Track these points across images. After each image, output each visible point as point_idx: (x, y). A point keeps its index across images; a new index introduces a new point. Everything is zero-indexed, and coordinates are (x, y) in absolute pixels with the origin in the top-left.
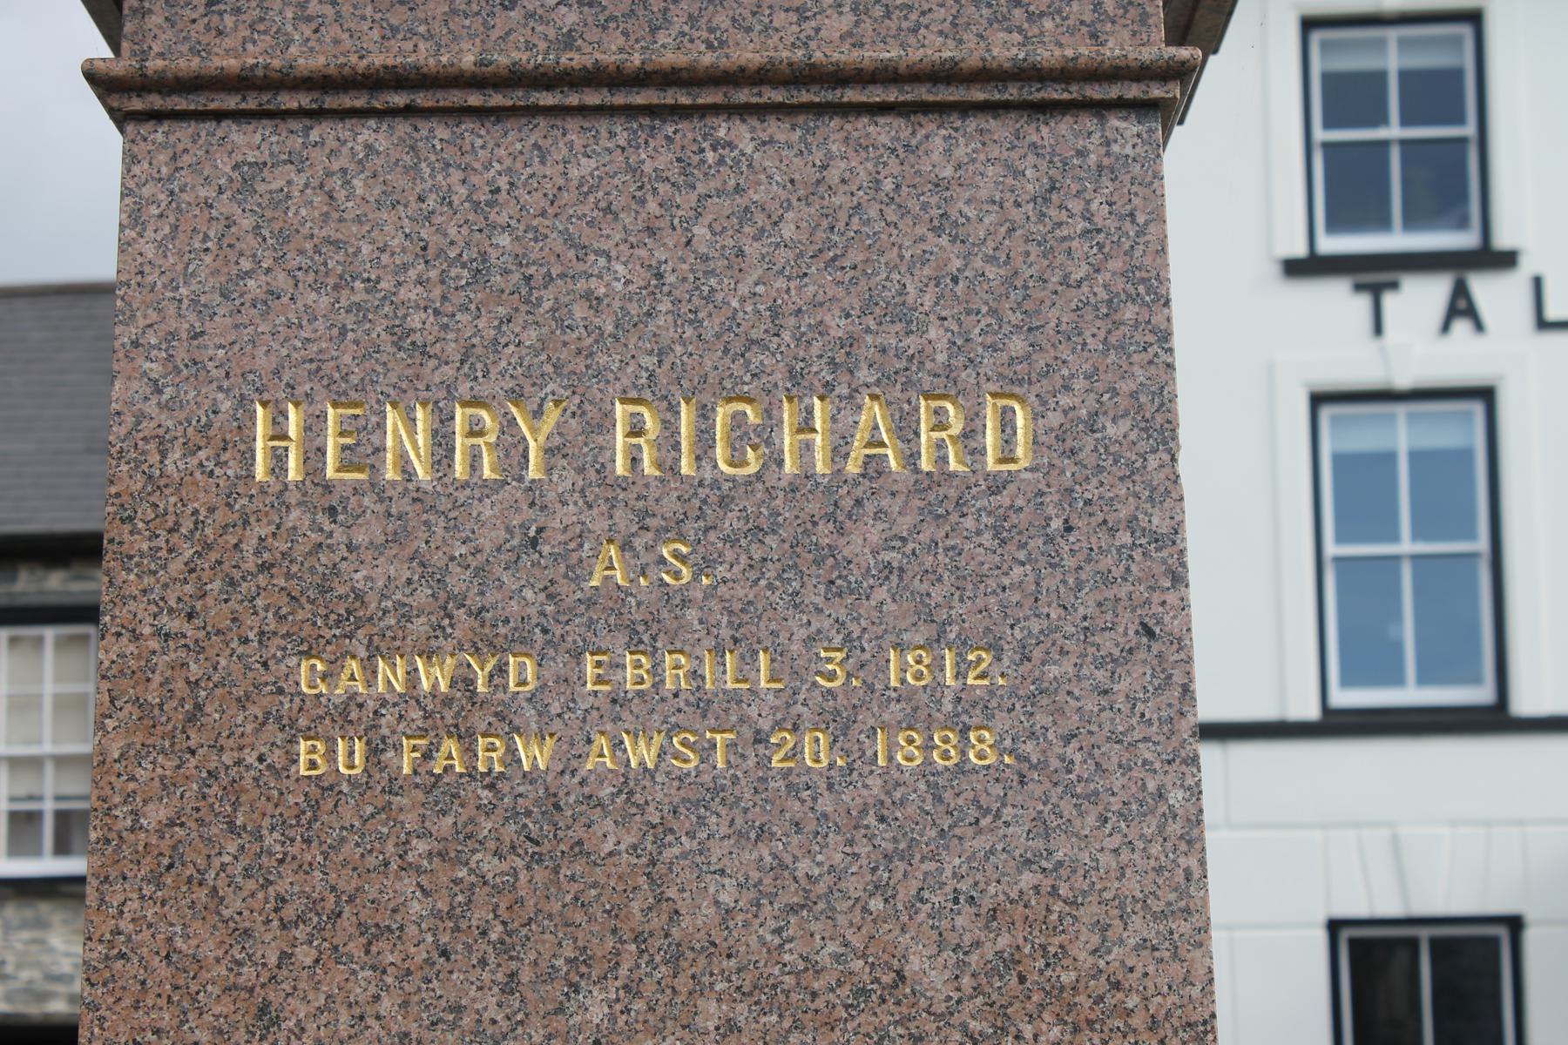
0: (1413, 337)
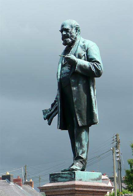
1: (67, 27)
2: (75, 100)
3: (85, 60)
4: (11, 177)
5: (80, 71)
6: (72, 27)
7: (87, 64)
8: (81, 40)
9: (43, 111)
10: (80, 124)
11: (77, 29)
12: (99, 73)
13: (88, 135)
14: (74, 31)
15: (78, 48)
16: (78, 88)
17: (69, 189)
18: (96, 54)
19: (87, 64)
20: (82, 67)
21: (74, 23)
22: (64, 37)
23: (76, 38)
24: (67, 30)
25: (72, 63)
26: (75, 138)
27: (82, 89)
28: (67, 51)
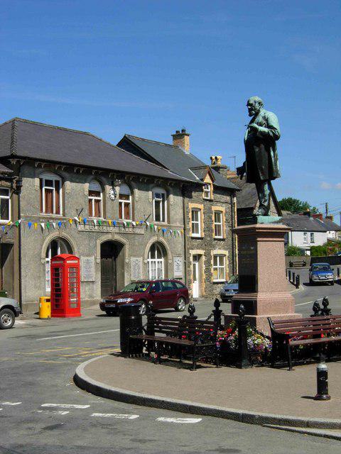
0: (245, 296)
1: (251, 102)
2: (257, 159)
3: (265, 127)
4: (315, 245)
5: (261, 136)
6: (255, 102)
7: (266, 130)
8: (263, 112)
9: (329, 398)
10: (262, 178)
11: (259, 103)
12: (277, 137)
13: (215, 450)
14: (257, 104)
15: (260, 119)
16: (260, 150)
17: (297, 429)
18: (274, 121)
19: (266, 130)
20: (262, 133)
21: (257, 99)
22: (250, 110)
23: (259, 111)
24: (251, 105)
25: (256, 130)
26: (260, 190)
27: (263, 150)
28: (252, 121)
